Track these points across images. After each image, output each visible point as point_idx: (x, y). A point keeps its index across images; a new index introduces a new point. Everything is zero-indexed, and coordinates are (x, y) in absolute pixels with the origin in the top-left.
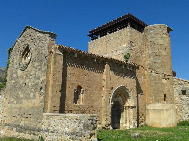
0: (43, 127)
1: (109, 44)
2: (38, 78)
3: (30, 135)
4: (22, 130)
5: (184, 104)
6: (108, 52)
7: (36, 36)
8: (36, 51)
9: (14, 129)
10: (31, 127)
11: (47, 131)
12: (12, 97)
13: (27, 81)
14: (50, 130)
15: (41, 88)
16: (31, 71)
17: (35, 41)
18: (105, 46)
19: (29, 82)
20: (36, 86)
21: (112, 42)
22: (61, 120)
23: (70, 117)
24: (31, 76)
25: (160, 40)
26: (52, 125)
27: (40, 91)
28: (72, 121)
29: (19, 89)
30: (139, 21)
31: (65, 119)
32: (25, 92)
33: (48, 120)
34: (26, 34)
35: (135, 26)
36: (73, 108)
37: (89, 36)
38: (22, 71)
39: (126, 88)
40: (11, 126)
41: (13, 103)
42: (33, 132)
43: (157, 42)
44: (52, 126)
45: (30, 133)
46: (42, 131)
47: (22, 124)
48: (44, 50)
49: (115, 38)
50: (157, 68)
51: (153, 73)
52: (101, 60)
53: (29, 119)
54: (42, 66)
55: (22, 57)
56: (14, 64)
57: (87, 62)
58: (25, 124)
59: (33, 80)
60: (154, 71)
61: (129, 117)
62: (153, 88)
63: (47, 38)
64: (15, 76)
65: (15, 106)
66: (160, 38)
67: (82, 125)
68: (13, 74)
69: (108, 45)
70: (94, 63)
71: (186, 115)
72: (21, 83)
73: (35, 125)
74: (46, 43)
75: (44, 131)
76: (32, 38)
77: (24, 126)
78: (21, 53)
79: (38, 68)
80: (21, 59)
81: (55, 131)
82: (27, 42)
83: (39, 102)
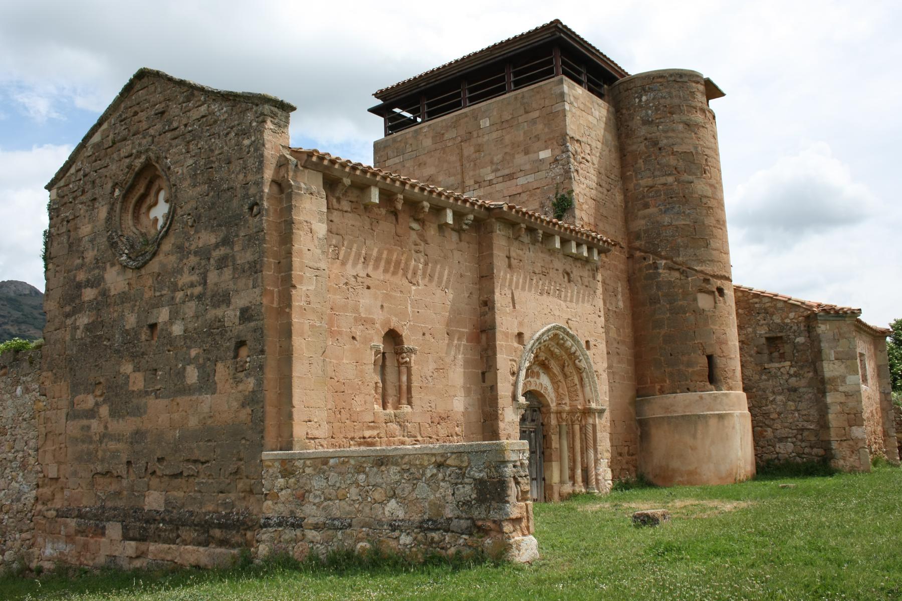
0: (270, 509)
1: (472, 149)
2: (223, 301)
3: (202, 549)
4: (157, 528)
5: (776, 389)
6: (472, 182)
7: (195, 114)
8: (200, 179)
9: (114, 530)
10: (205, 514)
11: (293, 525)
12: (88, 392)
13: (163, 315)
14: (311, 520)
15: (241, 344)
16: (180, 271)
17: (189, 137)
18: (454, 158)
19: (171, 321)
20: (210, 334)
21: (486, 138)
22: (362, 477)
23: (406, 459)
24: (179, 295)
25: (680, 135)
26: (316, 497)
27: (236, 356)
28: (417, 475)
29: (117, 351)
30: (593, 54)
31: (383, 468)
32: (155, 366)
33: (293, 480)
34: (136, 108)
35: (579, 73)
36: (373, 428)
37: (375, 110)
38: (129, 274)
39: (568, 334)
40: (93, 522)
41: (92, 414)
42: (217, 533)
43: (671, 141)
44: (317, 500)
45: (202, 538)
46: (266, 525)
47: (154, 501)
48: (241, 177)
49: (503, 124)
50: (676, 249)
51: (660, 271)
52: (471, 217)
53: (191, 480)
54: (236, 248)
55: (124, 209)
56: (80, 240)
57: (415, 226)
58: (167, 502)
59: (190, 308)
60: (663, 262)
61: (582, 453)
62: (663, 332)
63: (254, 124)
64: (89, 294)
65: (106, 427)
66: (681, 127)
67: (468, 488)
68: (79, 286)
69: (469, 150)
70: (442, 227)
71: (784, 432)
72: (127, 327)
73: (225, 505)
74: (246, 142)
75: (279, 524)
76: (175, 124)
77: (166, 511)
78: (117, 192)
79: (216, 254)
80: (118, 219)
81: (336, 523)
82: (144, 142)
83: (235, 404)
